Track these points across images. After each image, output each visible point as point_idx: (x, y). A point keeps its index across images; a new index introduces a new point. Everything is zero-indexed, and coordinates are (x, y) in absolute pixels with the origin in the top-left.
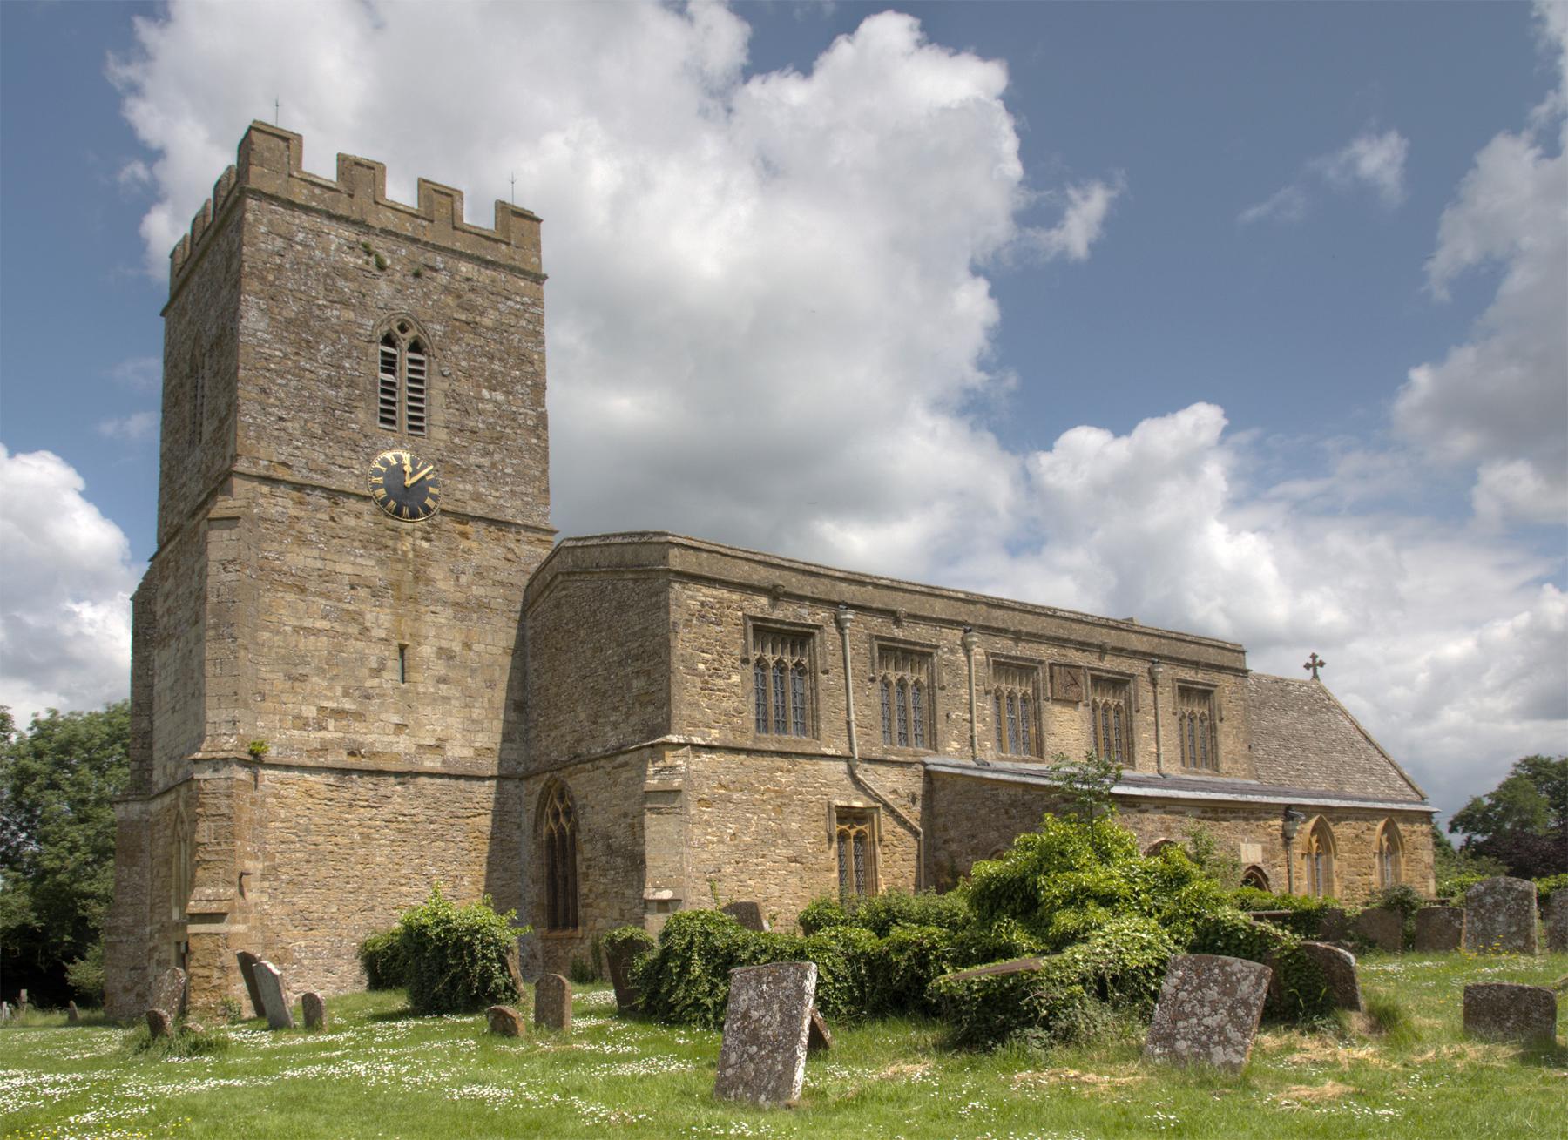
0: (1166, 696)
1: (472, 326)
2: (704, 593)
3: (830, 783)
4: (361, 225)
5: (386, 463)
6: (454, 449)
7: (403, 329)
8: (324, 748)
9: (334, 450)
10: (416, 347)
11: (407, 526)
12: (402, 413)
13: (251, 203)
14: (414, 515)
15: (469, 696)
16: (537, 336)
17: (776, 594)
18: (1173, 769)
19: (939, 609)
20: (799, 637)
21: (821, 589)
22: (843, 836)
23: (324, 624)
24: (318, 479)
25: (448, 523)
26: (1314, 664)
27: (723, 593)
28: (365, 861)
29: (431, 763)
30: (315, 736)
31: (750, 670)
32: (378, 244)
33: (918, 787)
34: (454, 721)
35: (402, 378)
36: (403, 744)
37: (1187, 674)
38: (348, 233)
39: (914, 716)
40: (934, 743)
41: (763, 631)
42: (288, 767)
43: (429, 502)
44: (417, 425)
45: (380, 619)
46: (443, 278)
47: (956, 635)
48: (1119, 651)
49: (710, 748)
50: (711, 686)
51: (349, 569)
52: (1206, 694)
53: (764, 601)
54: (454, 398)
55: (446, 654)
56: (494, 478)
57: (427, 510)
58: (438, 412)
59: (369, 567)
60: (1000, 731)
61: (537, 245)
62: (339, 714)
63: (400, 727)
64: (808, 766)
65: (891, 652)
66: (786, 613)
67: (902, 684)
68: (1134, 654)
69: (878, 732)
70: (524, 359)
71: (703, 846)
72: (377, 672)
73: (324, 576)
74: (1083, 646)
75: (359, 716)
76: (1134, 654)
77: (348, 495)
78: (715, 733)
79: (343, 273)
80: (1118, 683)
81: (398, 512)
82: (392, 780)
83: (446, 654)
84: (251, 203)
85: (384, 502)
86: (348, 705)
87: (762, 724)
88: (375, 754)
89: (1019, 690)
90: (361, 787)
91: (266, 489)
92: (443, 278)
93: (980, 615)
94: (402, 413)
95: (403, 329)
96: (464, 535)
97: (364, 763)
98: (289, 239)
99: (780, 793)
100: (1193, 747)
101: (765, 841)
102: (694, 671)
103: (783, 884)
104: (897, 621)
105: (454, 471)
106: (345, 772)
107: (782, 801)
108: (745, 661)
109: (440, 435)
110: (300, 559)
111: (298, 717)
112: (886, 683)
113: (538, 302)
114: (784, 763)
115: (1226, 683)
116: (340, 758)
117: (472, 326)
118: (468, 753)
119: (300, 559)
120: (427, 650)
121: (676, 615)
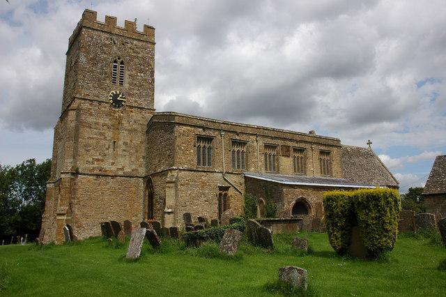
0: (316, 155)
1: (137, 57)
2: (184, 128)
3: (218, 180)
4: (110, 33)
5: (113, 93)
6: (130, 89)
7: (119, 59)
8: (94, 169)
9: (100, 90)
10: (122, 63)
11: (117, 110)
12: (118, 81)
13: (84, 29)
14: (119, 107)
15: (131, 154)
16: (153, 58)
17: (204, 128)
18: (318, 176)
19: (249, 131)
20: (209, 139)
21: (216, 126)
22: (220, 194)
23: (95, 136)
24: (97, 99)
25: (128, 109)
26: (369, 143)
27: (189, 128)
28: (102, 200)
29: (120, 173)
30: (91, 166)
31: (196, 149)
32: (114, 38)
33: (243, 181)
34: (127, 161)
35: (118, 71)
36: (113, 168)
37: (323, 148)
38: (107, 36)
39: (240, 161)
40: (306, 174)
41: (200, 138)
42: (84, 174)
43: (123, 103)
44: (121, 84)
45: (109, 134)
46: (129, 45)
47: (254, 138)
48: (301, 141)
49: (184, 170)
50: (186, 153)
51: (102, 122)
52: (328, 153)
53: (201, 130)
54: (131, 76)
55: (125, 143)
56: (140, 96)
57: (123, 105)
58: (127, 80)
59: (107, 121)
60: (266, 164)
61: (154, 35)
62: (98, 160)
63: (113, 164)
64: (211, 175)
65: (235, 143)
66: (207, 133)
67: (238, 151)
68: (306, 142)
69: (231, 165)
70: (149, 65)
71: (181, 197)
72: (107, 149)
73: (97, 123)
74: (291, 140)
75: (102, 160)
76: (306, 142)
77: (103, 102)
78: (186, 166)
79: (105, 45)
80: (302, 150)
81: (115, 106)
82: (110, 178)
83: (125, 143)
84: (84, 29)
85: (112, 104)
86: (100, 158)
87: (199, 163)
88: (106, 171)
89: (272, 153)
90: (102, 180)
91: (83, 101)
92: (129, 45)
93: (262, 132)
94: (118, 81)
95: (119, 59)
96: (132, 112)
97: (103, 173)
98: (92, 38)
99: (203, 183)
100: (324, 169)
101: (198, 196)
102: (180, 149)
103: (203, 207)
104: (238, 135)
105: (130, 95)
106: (98, 176)
107: (204, 185)
108: (195, 146)
109: (126, 85)
110: (91, 119)
111: (87, 161)
112: (234, 151)
113: (153, 50)
114: (205, 174)
115: (335, 150)
116: (96, 172)
117: (137, 57)
118: (130, 170)
119: (91, 119)
120: (121, 143)
121: (176, 134)
